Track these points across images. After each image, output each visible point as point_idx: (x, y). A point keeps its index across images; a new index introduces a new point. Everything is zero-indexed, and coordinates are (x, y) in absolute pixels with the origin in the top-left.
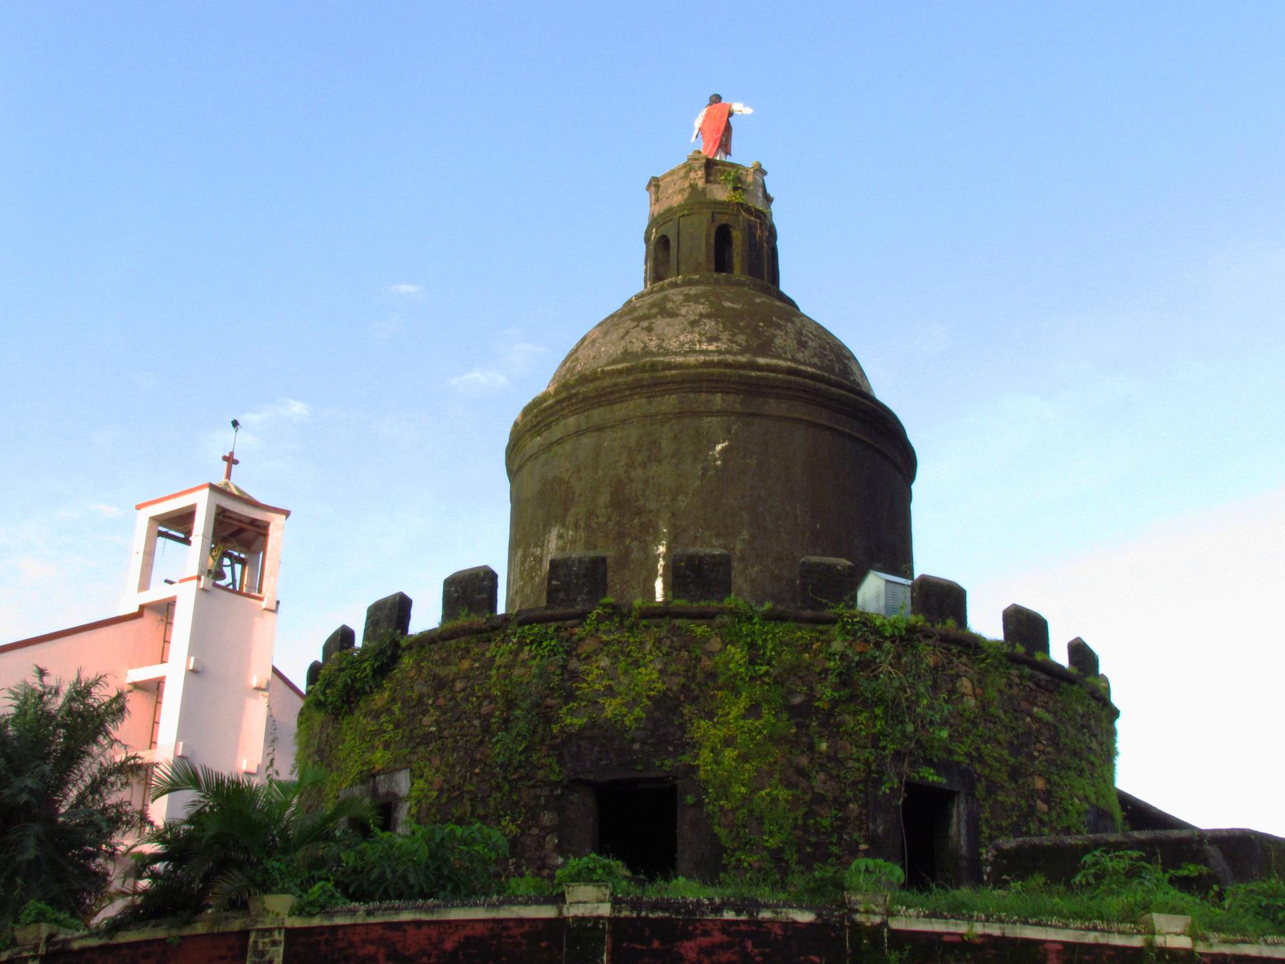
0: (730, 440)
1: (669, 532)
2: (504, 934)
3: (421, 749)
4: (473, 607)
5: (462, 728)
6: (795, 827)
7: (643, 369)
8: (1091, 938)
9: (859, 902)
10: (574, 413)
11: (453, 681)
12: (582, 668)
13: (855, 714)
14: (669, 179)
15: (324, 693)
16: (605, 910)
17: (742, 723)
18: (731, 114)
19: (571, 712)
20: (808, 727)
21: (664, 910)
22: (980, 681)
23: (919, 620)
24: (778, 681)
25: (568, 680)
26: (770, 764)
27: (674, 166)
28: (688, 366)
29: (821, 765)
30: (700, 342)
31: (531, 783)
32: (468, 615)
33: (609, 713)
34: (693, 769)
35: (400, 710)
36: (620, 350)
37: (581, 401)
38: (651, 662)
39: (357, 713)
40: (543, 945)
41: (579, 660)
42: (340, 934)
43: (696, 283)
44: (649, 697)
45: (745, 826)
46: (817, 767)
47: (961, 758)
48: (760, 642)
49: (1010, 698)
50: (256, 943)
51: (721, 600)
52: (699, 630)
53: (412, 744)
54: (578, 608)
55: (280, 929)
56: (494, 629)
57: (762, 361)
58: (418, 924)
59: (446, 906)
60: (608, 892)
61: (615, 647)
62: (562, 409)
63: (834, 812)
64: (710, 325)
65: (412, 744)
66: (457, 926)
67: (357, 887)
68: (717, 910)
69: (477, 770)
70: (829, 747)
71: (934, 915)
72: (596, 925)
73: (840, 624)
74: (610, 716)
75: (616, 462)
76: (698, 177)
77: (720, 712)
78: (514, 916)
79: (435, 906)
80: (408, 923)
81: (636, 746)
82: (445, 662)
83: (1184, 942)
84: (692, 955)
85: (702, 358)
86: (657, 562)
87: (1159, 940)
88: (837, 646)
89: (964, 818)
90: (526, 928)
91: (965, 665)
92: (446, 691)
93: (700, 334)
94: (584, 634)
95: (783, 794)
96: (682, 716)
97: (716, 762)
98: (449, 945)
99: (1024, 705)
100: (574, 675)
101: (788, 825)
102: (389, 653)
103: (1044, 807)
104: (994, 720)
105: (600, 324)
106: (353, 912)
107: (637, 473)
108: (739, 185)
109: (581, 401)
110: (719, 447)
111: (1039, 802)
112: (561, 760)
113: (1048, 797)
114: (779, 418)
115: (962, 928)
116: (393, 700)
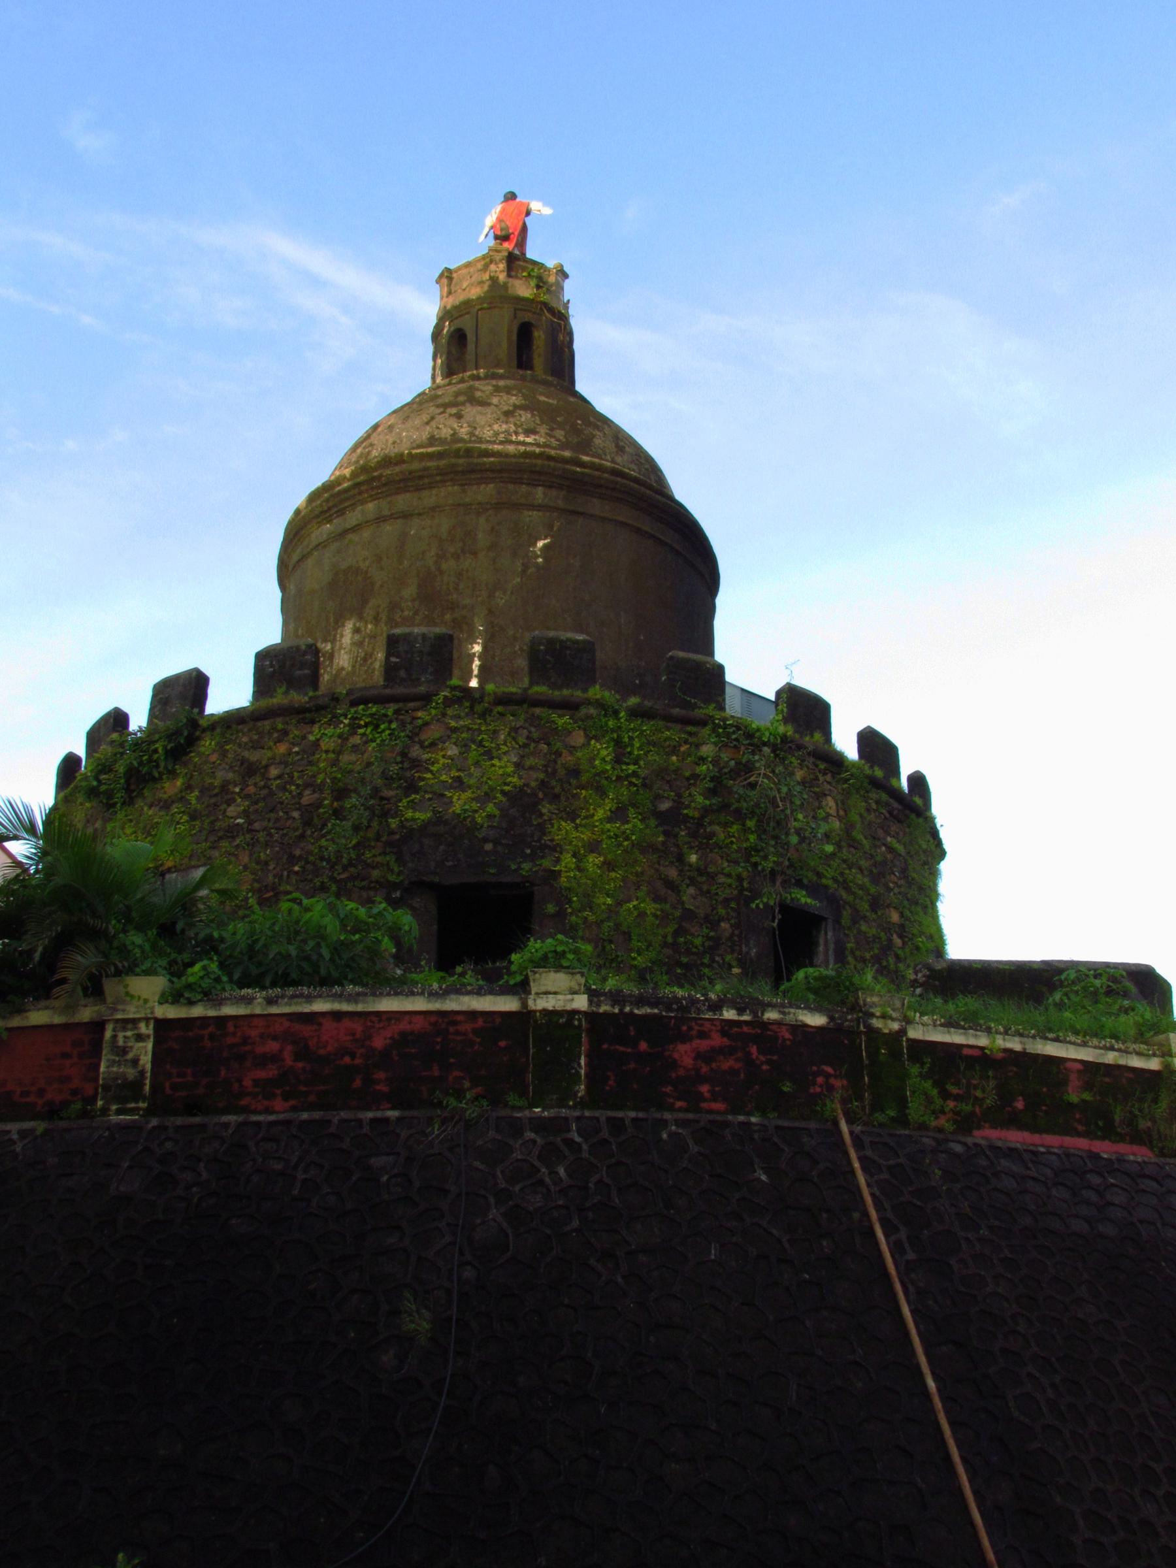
0: (552, 537)
1: (486, 631)
2: (451, 1029)
3: (224, 844)
4: (292, 683)
5: (278, 820)
6: (665, 944)
7: (457, 454)
8: (1110, 1058)
9: (874, 1005)
10: (373, 498)
11: (267, 767)
12: (426, 756)
13: (726, 825)
14: (464, 271)
15: (97, 778)
16: (581, 1002)
17: (608, 826)
18: (528, 213)
19: (413, 805)
20: (676, 836)
21: (652, 1005)
22: (843, 803)
23: (789, 730)
25: (410, 769)
26: (637, 874)
27: (471, 258)
28: (507, 455)
29: (690, 878)
30: (516, 433)
31: (364, 883)
32: (286, 693)
33: (457, 808)
34: (555, 875)
35: (198, 798)
36: (425, 435)
37: (384, 485)
38: (505, 753)
39: (140, 803)
40: (502, 1044)
41: (422, 747)
42: (231, 1027)
43: (501, 377)
44: (503, 793)
45: (611, 942)
46: (688, 881)
47: (830, 882)
48: (626, 740)
49: (870, 823)
50: (115, 1037)
51: (585, 690)
52: (560, 722)
53: (212, 838)
54: (422, 689)
55: (147, 1020)
56: (320, 708)
57: (585, 458)
58: (337, 1016)
59: (374, 995)
60: (583, 981)
61: (464, 735)
62: (360, 493)
63: (705, 931)
64: (525, 416)
65: (212, 838)
66: (389, 1019)
67: (252, 969)
68: (716, 1007)
69: (296, 868)
70: (698, 859)
72: (569, 1023)
73: (709, 727)
74: (458, 811)
75: (424, 552)
76: (499, 270)
77: (584, 813)
78: (464, 1008)
79: (358, 994)
80: (323, 1014)
81: (489, 847)
82: (256, 746)
84: (688, 1061)
85: (522, 448)
86: (472, 661)
88: (707, 750)
89: (832, 946)
90: (480, 1022)
91: (829, 783)
92: (258, 779)
93: (515, 425)
94: (428, 718)
95: (650, 907)
96: (541, 815)
97: (579, 869)
98: (379, 1043)
99: (880, 833)
100: (416, 764)
102: (186, 733)
104: (854, 844)
105: (395, 412)
106: (249, 1000)
107: (449, 565)
108: (541, 283)
109: (384, 485)
110: (540, 544)
111: (895, 936)
112: (400, 860)
114: (603, 519)
115: (983, 1041)
116: (189, 787)
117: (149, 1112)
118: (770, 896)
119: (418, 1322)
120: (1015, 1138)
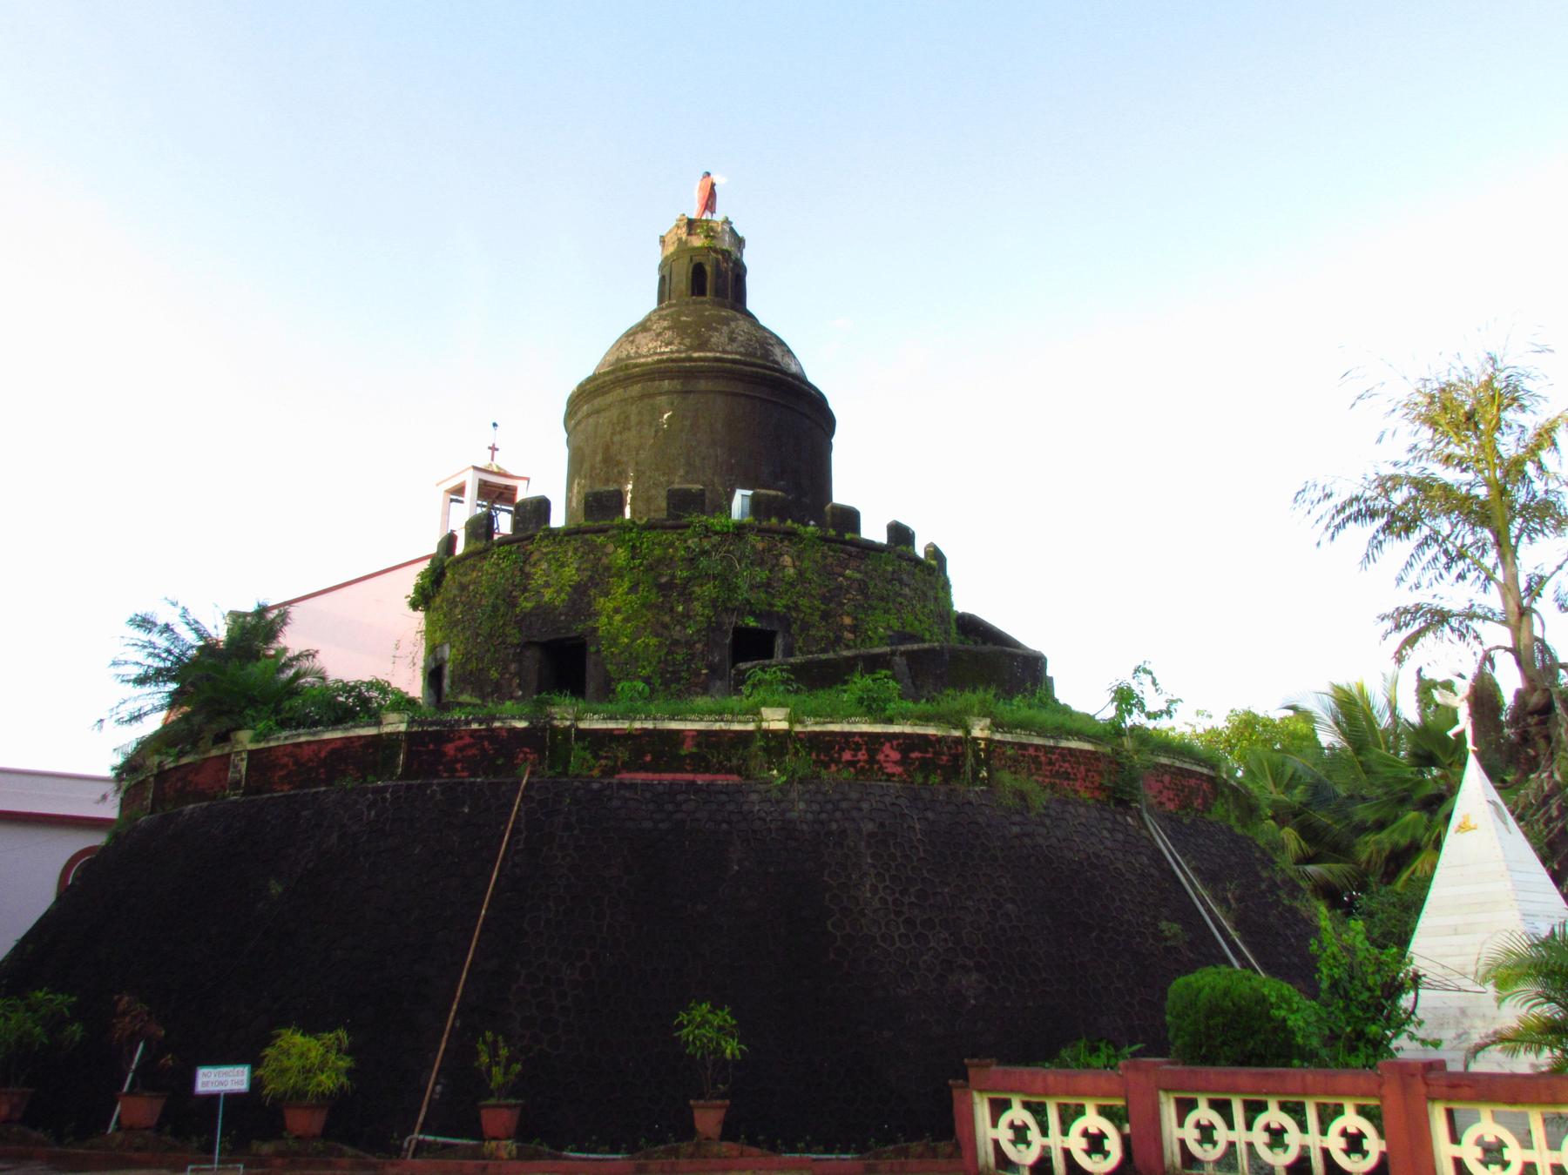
8: (717, 726)
16: (403, 727)
24: (651, 568)
28: (647, 364)
33: (546, 599)
34: (595, 630)
64: (669, 334)
68: (468, 723)
71: (612, 718)
83: (784, 725)
84: (452, 752)
87: (765, 725)
95: (654, 641)
98: (323, 755)
99: (838, 570)
101: (654, 661)
103: (851, 636)
112: (520, 631)
113: (854, 629)
115: (625, 725)
117: (243, 794)
118: (730, 621)
119: (276, 888)
120: (640, 777)
